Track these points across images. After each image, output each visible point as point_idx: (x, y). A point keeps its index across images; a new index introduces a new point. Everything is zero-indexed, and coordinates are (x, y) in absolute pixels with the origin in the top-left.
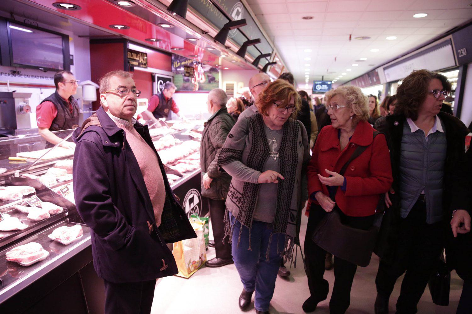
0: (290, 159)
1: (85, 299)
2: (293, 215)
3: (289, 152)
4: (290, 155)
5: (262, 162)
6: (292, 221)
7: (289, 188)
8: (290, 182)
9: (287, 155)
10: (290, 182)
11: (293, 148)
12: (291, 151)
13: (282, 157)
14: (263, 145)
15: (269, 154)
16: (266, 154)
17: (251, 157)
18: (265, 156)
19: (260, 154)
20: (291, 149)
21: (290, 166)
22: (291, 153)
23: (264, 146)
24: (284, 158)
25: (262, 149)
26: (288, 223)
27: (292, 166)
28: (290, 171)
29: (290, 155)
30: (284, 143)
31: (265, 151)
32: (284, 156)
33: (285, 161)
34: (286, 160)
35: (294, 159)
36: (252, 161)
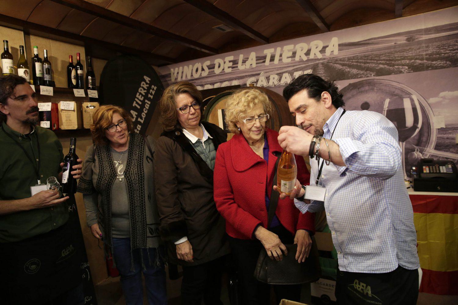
0: (136, 178)
1: (219, 94)
2: (151, 229)
3: (135, 171)
4: (136, 174)
5: (109, 185)
6: (151, 234)
7: (140, 205)
8: (140, 200)
9: (133, 175)
10: (140, 200)
11: (139, 165)
12: (136, 169)
13: (128, 177)
14: (109, 170)
15: (115, 177)
16: (112, 177)
17: (98, 183)
18: (111, 180)
19: (107, 178)
20: (136, 167)
21: (138, 184)
22: (137, 171)
23: (110, 170)
24: (130, 178)
25: (108, 173)
26: (147, 237)
27: (139, 184)
28: (138, 189)
29: (136, 174)
30: (129, 163)
31: (111, 174)
32: (130, 176)
33: (131, 180)
34: (132, 179)
35: (139, 177)
36: (100, 186)
